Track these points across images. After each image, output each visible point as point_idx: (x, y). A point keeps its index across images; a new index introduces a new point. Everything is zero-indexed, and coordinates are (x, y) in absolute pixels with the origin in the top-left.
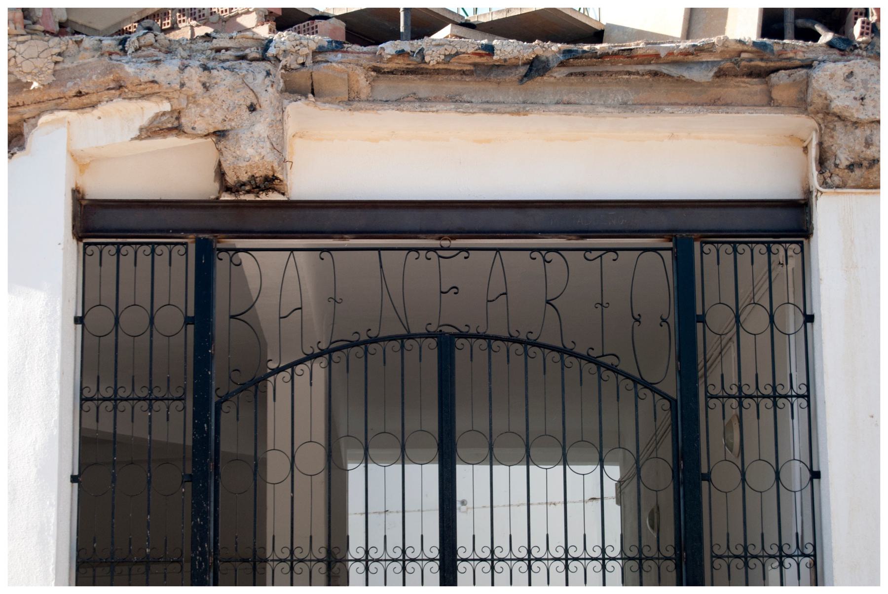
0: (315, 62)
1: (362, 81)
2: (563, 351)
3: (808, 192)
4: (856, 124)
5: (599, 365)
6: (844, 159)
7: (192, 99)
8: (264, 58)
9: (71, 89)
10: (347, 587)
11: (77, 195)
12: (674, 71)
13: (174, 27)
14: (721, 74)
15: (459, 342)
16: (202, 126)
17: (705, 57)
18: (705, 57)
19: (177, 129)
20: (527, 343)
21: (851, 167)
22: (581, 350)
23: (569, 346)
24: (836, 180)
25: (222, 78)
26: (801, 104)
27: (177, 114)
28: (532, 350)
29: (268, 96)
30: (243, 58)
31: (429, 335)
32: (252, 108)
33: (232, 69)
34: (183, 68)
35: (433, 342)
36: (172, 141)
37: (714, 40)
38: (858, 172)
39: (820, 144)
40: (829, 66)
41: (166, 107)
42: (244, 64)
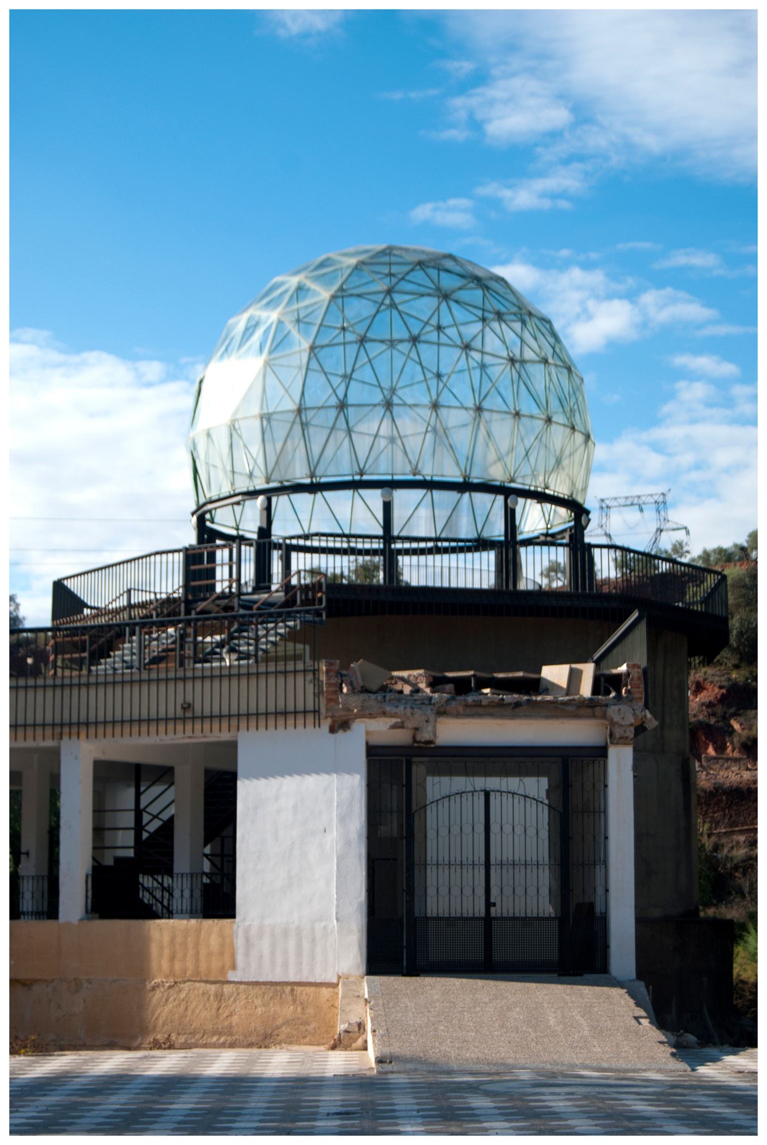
0: (447, 704)
1: (461, 709)
2: (525, 796)
3: (607, 743)
4: (622, 726)
5: (537, 801)
6: (618, 736)
7: (408, 718)
8: (430, 704)
9: (367, 712)
10: (759, 1075)
11: (367, 743)
12: (563, 707)
13: (396, 683)
14: (578, 707)
15: (491, 793)
16: (410, 726)
17: (573, 702)
18: (573, 702)
19: (403, 727)
20: (514, 794)
21: (620, 738)
22: (531, 796)
23: (527, 794)
24: (615, 742)
25: (418, 712)
26: (604, 717)
27: (403, 722)
28: (515, 796)
29: (432, 717)
30: (423, 704)
31: (482, 791)
32: (427, 721)
33: (420, 708)
34: (405, 708)
35: (483, 793)
36: (400, 730)
37: (576, 697)
38: (622, 740)
39: (610, 730)
40: (613, 707)
41: (399, 720)
42: (424, 706)
